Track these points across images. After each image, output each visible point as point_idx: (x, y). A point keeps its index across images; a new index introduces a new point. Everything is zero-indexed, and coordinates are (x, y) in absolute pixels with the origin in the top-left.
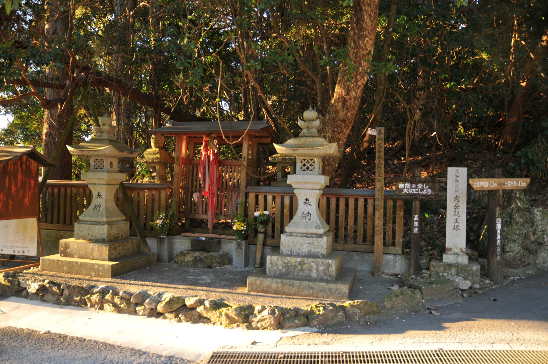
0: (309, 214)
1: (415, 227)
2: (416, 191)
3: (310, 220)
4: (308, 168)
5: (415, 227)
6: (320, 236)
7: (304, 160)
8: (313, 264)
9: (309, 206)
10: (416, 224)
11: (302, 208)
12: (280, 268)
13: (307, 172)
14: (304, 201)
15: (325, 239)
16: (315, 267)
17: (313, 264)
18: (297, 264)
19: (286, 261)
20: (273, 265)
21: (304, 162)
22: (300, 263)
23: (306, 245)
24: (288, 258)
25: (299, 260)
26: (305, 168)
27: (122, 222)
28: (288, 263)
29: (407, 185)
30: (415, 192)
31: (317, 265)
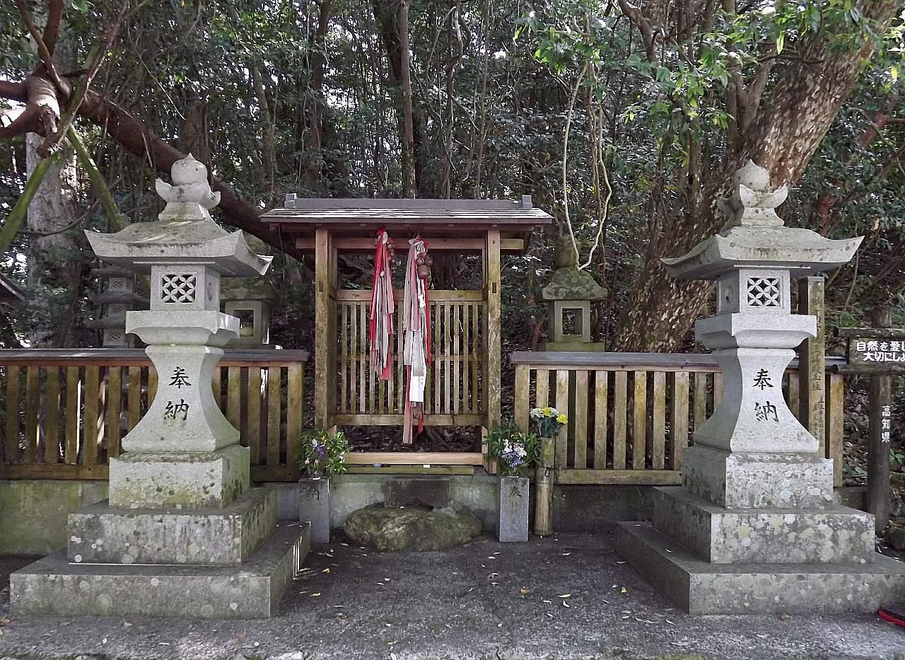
0: (770, 407)
1: (886, 430)
2: (888, 356)
3: (776, 420)
4: (763, 299)
5: (886, 430)
6: (205, 457)
7: (755, 280)
8: (822, 527)
9: (765, 388)
10: (886, 424)
11: (165, 393)
12: (746, 542)
13: (178, 302)
14: (756, 376)
15: (218, 465)
16: (829, 533)
17: (822, 527)
18: (786, 530)
19: (760, 525)
20: (729, 535)
21: (756, 285)
22: (794, 527)
23: (786, 483)
24: (765, 516)
25: (790, 518)
26: (171, 295)
27: (235, 448)
28: (764, 529)
29: (873, 344)
30: (886, 359)
31: (835, 528)
